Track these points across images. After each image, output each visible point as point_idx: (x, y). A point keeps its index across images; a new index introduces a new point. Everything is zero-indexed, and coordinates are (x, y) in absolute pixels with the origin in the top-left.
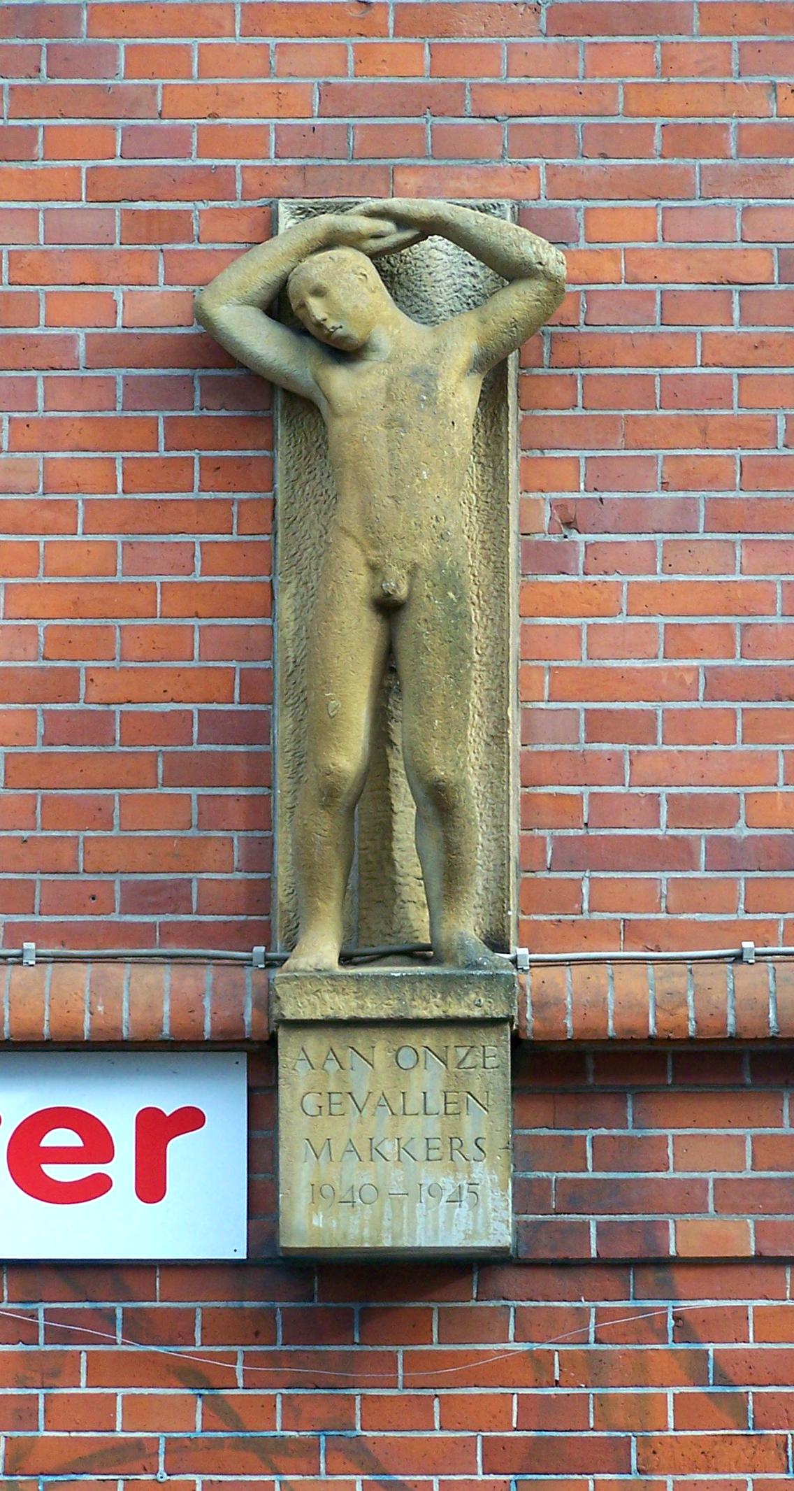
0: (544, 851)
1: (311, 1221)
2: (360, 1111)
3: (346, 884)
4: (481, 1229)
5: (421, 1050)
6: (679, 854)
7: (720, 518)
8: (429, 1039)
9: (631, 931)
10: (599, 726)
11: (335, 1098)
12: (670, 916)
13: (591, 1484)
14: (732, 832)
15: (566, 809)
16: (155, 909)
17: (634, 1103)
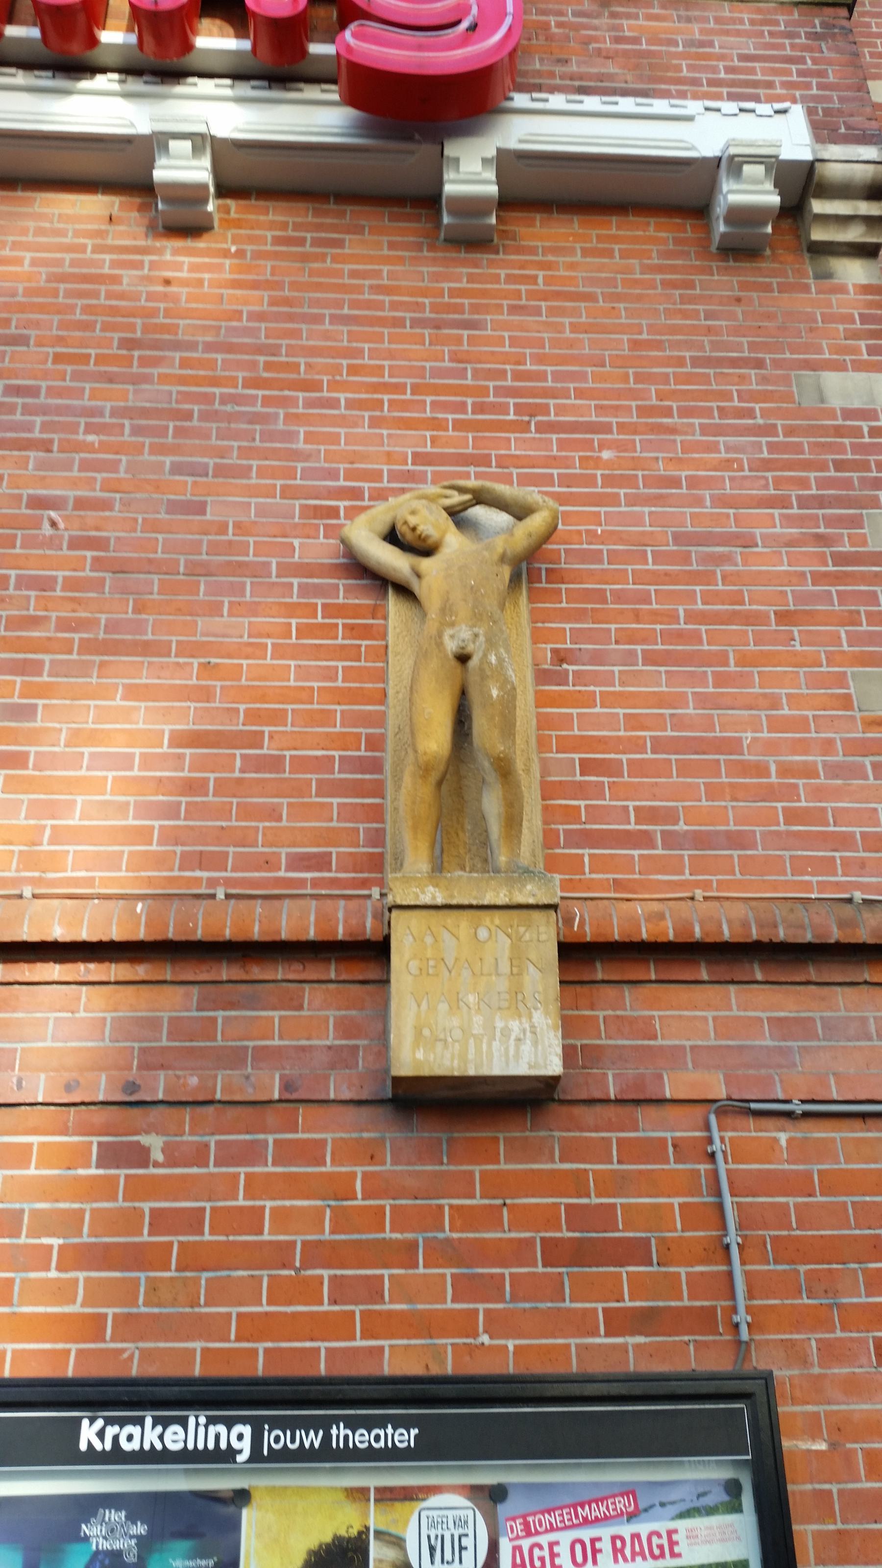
0: (559, 837)
1: (414, 1053)
2: (450, 972)
3: (433, 853)
4: (541, 1062)
5: (493, 928)
6: (643, 840)
7: (650, 658)
8: (498, 918)
9: (618, 885)
10: (587, 767)
11: (431, 963)
12: (643, 877)
13: (625, 1275)
14: (676, 828)
15: (572, 814)
16: (308, 869)
17: (630, 992)
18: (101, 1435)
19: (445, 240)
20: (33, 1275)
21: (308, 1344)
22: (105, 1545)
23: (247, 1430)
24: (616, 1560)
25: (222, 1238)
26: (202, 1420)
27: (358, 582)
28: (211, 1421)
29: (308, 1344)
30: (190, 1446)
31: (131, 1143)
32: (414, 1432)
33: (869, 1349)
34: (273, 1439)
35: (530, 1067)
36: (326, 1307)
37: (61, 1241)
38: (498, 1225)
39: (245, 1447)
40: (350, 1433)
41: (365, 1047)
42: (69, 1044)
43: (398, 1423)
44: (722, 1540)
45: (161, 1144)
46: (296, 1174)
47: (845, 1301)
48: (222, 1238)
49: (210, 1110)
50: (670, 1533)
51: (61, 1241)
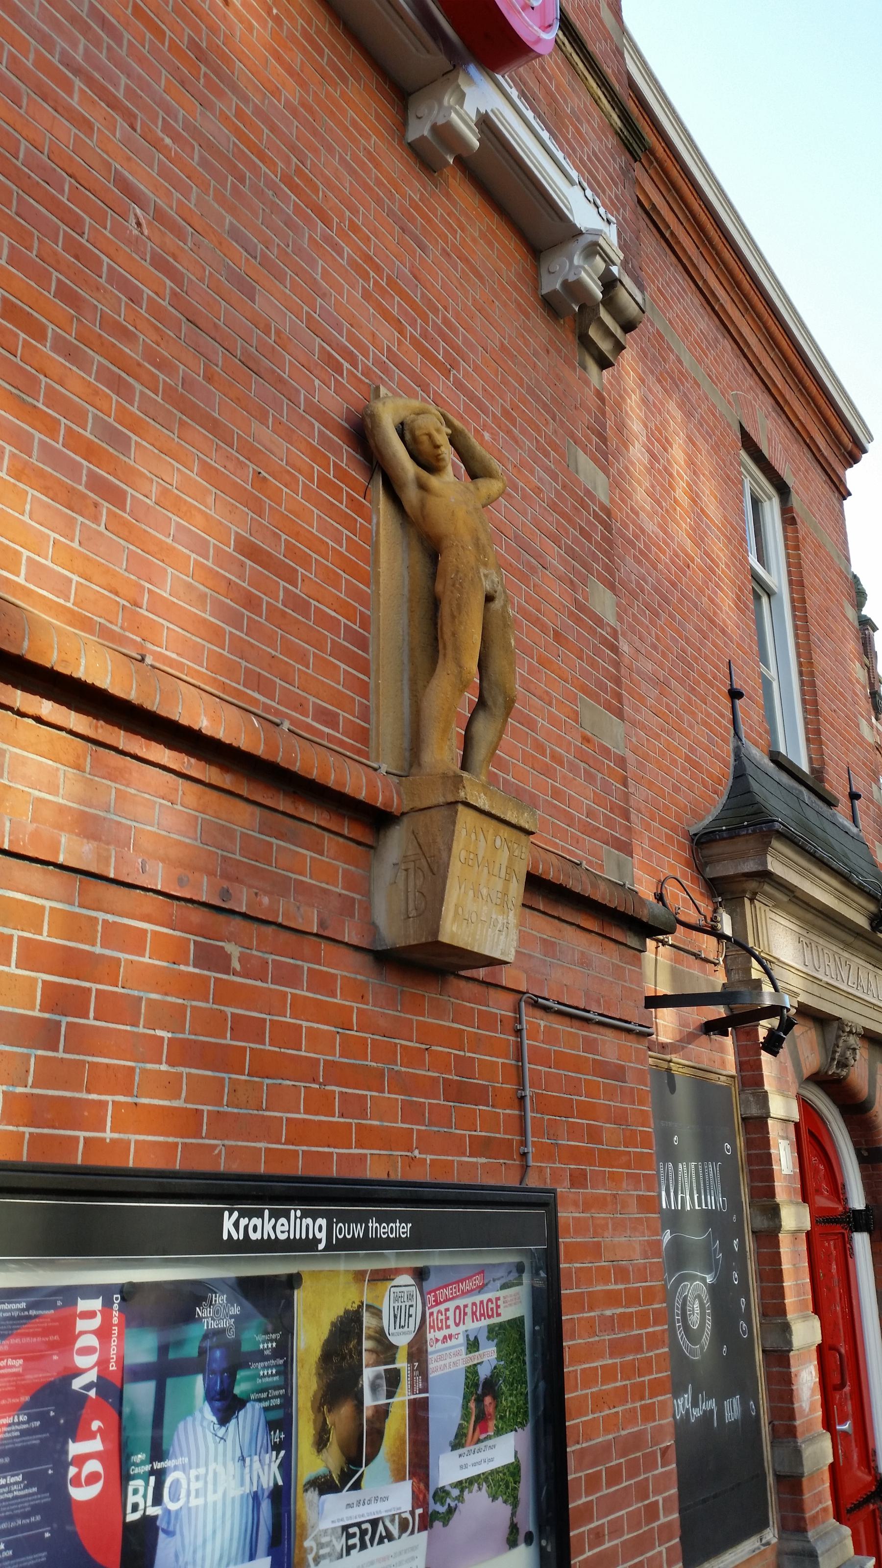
18: (236, 1225)
20: (149, 1066)
21: (326, 1150)
22: (214, 1325)
23: (322, 1222)
24: (473, 1321)
25: (277, 1049)
26: (299, 1213)
27: (354, 453)
28: (305, 1214)
29: (326, 1150)
30: (292, 1237)
31: (218, 946)
32: (410, 1225)
34: (342, 1231)
35: (502, 954)
36: (336, 1119)
37: (170, 1035)
38: (421, 1065)
39: (322, 1235)
40: (377, 1225)
41: (360, 902)
42: (172, 835)
44: (515, 1304)
45: (238, 955)
46: (321, 1001)
48: (277, 1049)
49: (269, 930)
50: (498, 1299)
51: (170, 1035)
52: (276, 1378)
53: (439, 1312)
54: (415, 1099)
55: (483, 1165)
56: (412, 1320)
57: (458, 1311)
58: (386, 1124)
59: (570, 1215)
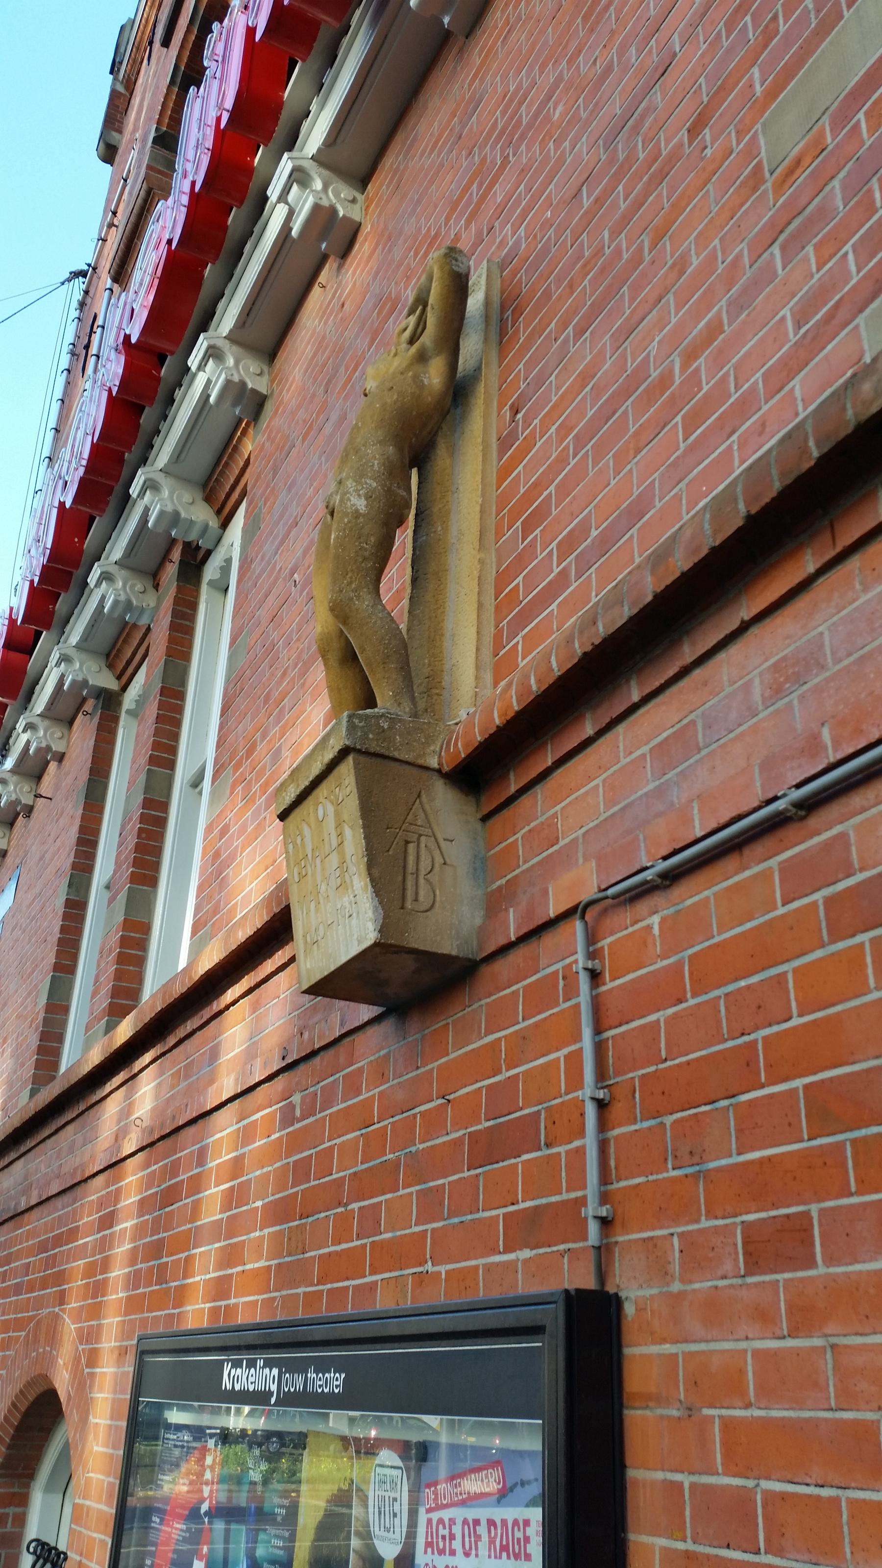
19: (362, 181)
23: (275, 1371)
24: (490, 1557)
32: (343, 1376)
33: (735, 1245)
43: (322, 1367)
47: (712, 1165)
52: (281, 1553)
53: (441, 1521)
54: (432, 1184)
55: (526, 1261)
56: (397, 1520)
57: (466, 1527)
58: (398, 1233)
59: (743, 1345)
